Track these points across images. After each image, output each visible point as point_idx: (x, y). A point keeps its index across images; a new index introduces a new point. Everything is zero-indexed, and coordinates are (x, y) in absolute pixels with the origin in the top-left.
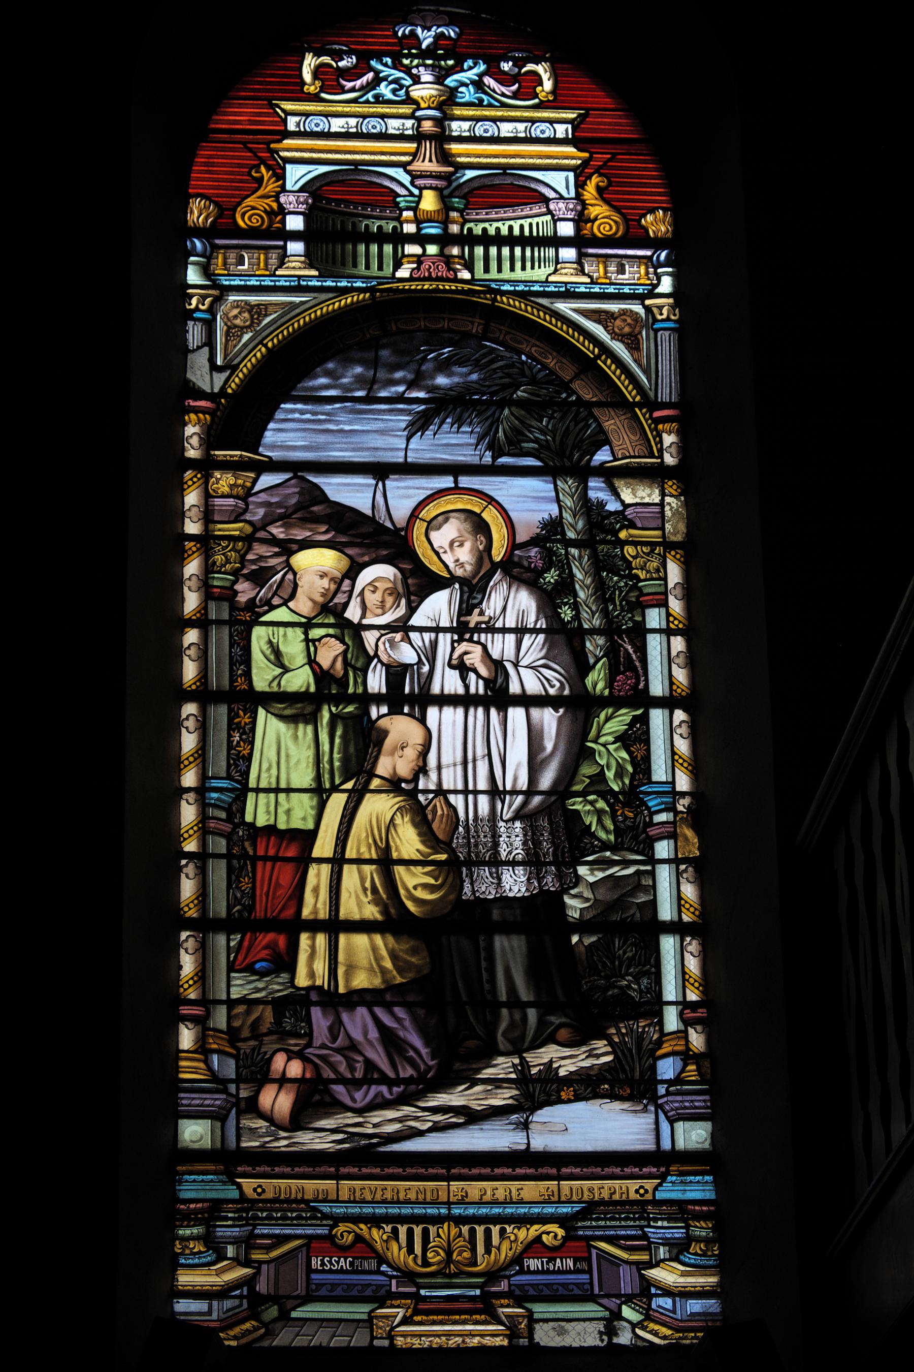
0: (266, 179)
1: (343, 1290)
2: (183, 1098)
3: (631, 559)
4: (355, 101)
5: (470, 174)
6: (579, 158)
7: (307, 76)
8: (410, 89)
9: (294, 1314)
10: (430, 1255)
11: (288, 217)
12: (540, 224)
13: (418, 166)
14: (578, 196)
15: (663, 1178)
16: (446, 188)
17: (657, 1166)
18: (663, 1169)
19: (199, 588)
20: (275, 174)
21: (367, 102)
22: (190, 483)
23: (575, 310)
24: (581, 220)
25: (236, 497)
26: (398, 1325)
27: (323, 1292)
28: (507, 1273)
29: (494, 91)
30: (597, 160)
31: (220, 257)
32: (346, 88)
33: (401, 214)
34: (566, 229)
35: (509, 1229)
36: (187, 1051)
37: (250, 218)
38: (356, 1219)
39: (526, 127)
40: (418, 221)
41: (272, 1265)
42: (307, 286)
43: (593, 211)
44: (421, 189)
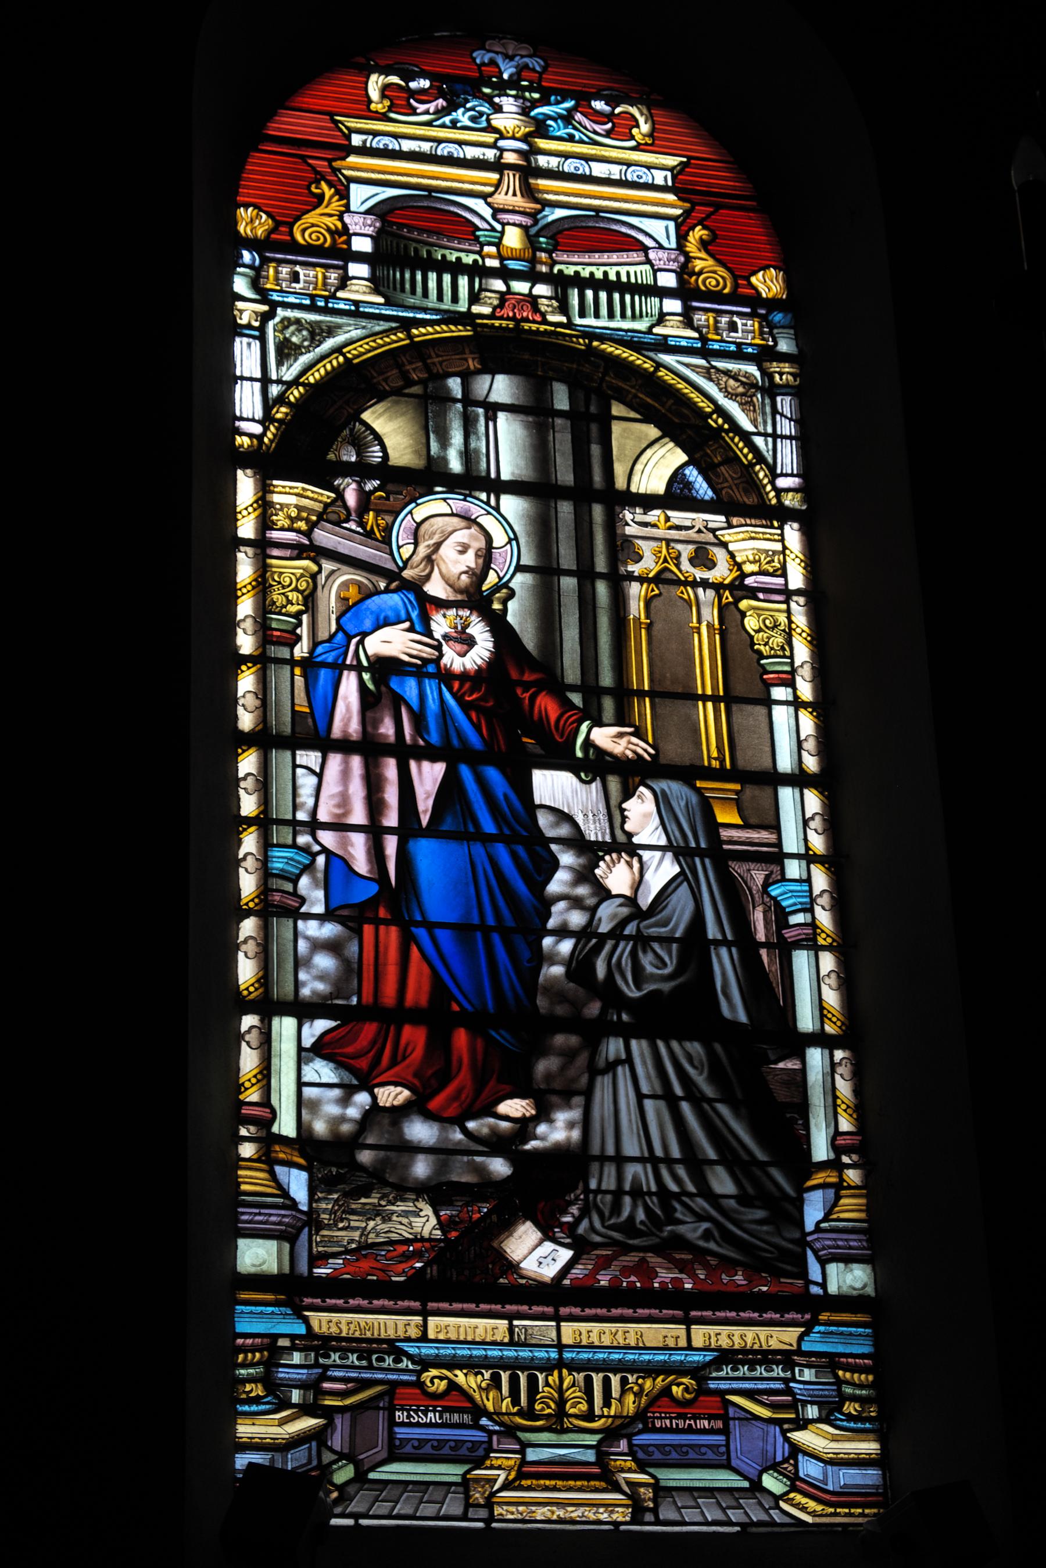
0: (327, 197)
1: (433, 1447)
2: (243, 1213)
3: (753, 633)
4: (429, 124)
5: (560, 213)
6: (680, 207)
7: (374, 93)
8: (491, 117)
9: (372, 1476)
10: (538, 1407)
11: (354, 238)
12: (641, 273)
13: (500, 199)
14: (681, 247)
15: (809, 1327)
16: (532, 226)
17: (802, 1312)
18: (808, 1316)
19: (256, 631)
20: (337, 192)
21: (443, 126)
22: (245, 513)
23: (678, 362)
24: (684, 272)
25: (298, 531)
26: (500, 1490)
27: (408, 1449)
28: (629, 1430)
29: (586, 128)
30: (700, 212)
31: (271, 271)
32: (418, 111)
33: (482, 249)
34: (668, 280)
35: (631, 1379)
36: (249, 1160)
37: (310, 235)
38: (453, 1364)
39: (432, 147)
40: (501, 258)
41: (347, 1416)
42: (333, 308)
43: (699, 265)
44: (503, 225)
